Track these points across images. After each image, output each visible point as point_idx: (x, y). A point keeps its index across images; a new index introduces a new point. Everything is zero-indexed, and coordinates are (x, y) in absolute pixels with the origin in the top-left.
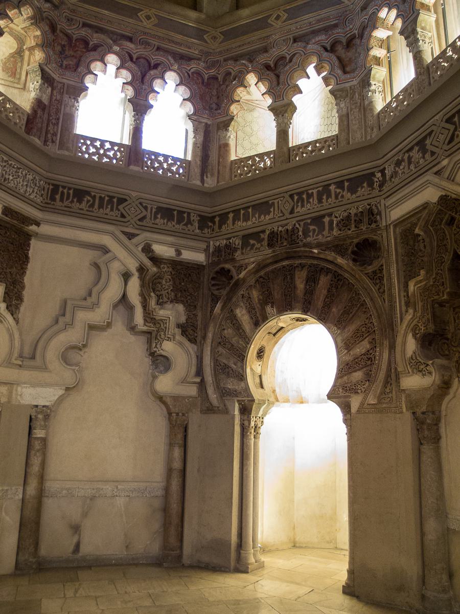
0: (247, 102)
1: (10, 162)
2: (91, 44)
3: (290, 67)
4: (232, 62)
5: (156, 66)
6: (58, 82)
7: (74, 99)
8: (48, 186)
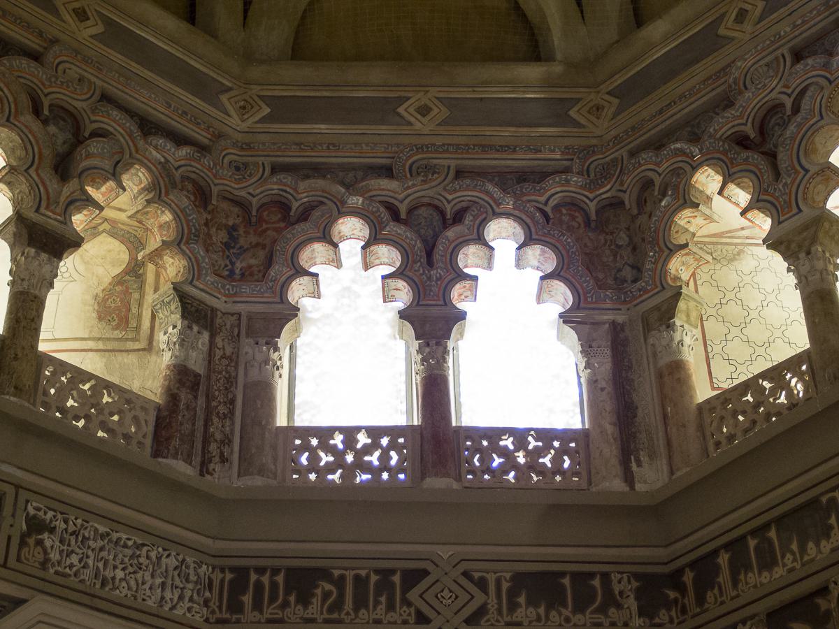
0: (714, 240)
1: (115, 536)
2: (294, 208)
3: (800, 126)
4: (651, 154)
5: (458, 218)
6: (224, 314)
7: (267, 343)
8: (220, 576)
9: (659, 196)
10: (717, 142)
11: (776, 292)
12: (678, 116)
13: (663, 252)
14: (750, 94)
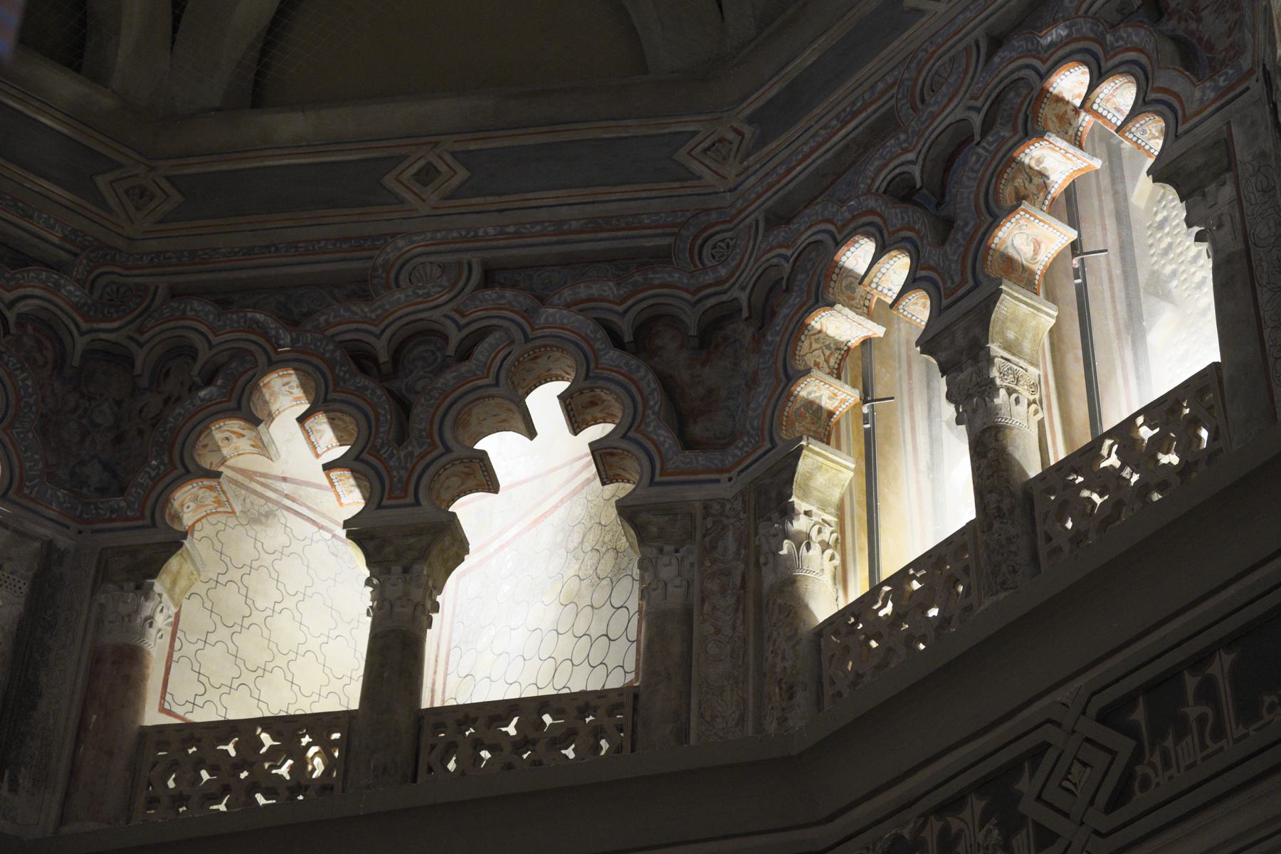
0: (240, 478)
4: (208, 308)
9: (197, 379)
10: (325, 342)
11: (300, 596)
12: (273, 271)
13: (175, 468)
14: (403, 296)
